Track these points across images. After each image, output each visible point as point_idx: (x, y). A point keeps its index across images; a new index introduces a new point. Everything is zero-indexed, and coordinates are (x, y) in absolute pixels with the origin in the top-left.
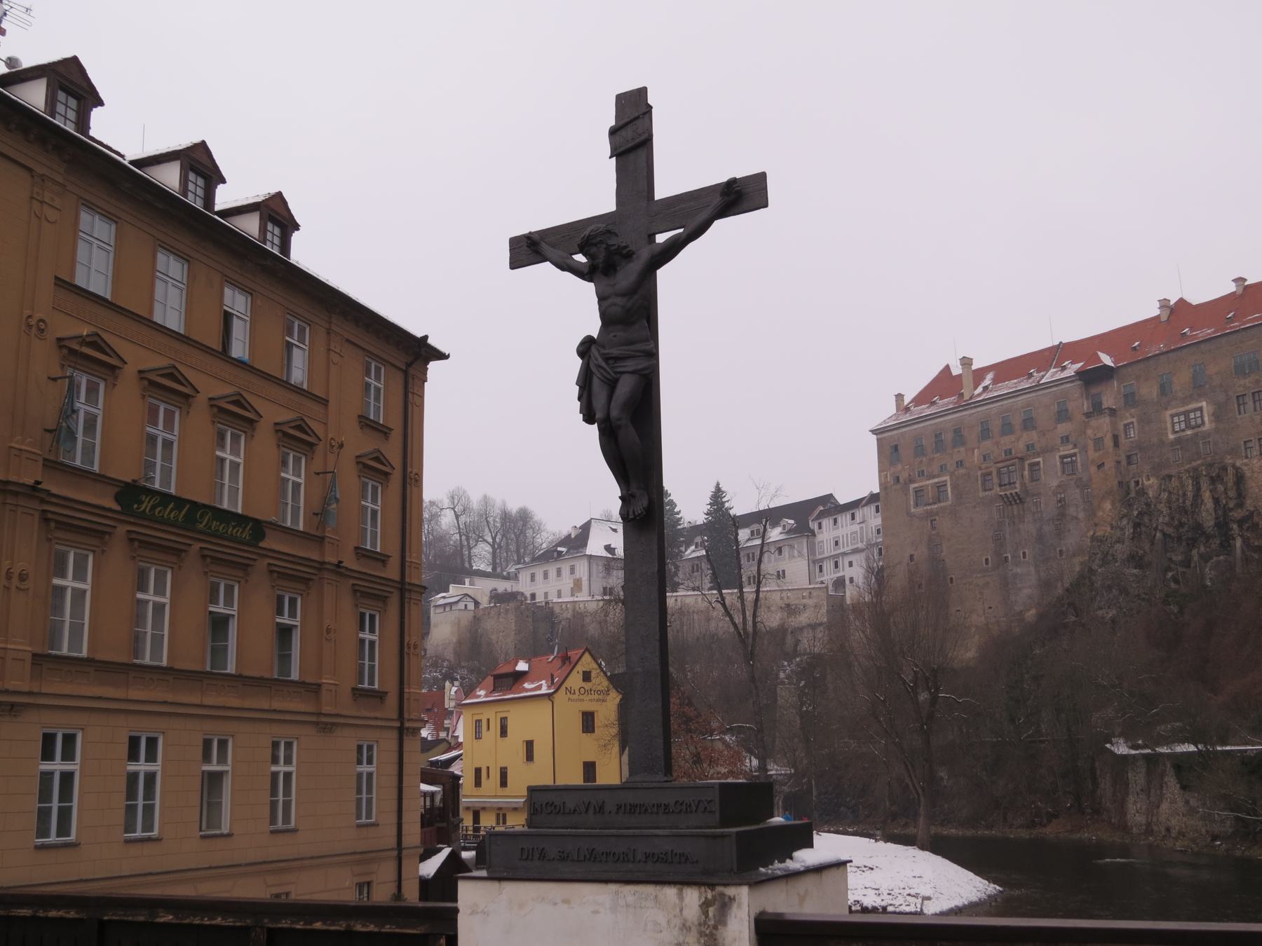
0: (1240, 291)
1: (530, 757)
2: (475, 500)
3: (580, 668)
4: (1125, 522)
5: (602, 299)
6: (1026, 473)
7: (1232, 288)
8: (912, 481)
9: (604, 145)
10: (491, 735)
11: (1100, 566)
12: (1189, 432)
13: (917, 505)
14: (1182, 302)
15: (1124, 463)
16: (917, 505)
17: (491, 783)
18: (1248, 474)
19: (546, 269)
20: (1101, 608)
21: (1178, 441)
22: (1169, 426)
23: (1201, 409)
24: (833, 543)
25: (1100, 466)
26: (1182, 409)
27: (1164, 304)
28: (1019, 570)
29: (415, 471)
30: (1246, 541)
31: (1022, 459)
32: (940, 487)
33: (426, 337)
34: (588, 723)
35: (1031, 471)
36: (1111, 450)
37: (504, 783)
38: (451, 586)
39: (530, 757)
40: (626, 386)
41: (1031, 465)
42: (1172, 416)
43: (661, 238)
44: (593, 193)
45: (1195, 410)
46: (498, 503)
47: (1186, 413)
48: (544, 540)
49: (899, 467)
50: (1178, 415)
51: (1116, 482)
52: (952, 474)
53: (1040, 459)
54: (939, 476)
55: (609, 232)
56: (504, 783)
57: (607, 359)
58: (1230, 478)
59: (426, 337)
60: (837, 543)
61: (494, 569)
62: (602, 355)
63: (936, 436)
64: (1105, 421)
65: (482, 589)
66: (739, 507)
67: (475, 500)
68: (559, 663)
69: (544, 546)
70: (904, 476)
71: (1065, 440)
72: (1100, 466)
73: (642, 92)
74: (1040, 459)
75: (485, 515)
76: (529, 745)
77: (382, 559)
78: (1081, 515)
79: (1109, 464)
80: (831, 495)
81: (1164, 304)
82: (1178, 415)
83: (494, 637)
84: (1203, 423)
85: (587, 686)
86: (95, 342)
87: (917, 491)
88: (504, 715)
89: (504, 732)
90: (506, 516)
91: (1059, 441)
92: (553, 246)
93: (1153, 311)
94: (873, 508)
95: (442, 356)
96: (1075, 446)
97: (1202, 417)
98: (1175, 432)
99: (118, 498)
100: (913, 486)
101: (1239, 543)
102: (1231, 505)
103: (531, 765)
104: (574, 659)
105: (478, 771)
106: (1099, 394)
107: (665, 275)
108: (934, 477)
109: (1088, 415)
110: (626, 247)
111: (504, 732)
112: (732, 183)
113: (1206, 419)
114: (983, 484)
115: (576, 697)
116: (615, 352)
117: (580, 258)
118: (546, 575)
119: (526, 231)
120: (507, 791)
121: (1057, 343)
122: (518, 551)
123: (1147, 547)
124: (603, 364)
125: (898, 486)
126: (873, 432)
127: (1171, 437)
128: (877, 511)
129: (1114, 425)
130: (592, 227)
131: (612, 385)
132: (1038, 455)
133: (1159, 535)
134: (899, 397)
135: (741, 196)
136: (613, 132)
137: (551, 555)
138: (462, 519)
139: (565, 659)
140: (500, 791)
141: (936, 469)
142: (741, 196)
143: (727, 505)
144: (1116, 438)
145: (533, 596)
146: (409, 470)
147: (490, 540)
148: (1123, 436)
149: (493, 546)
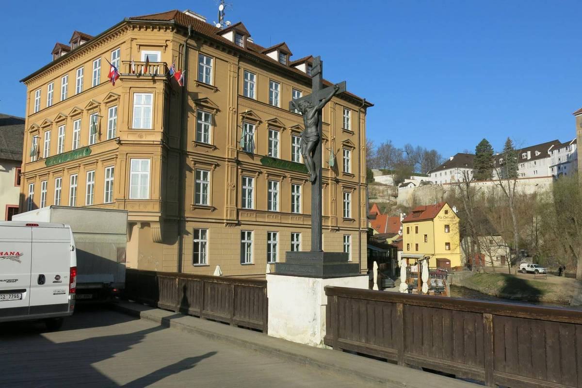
2: (415, 147)
24: (558, 159)
38: (405, 180)
46: (424, 149)
48: (442, 161)
56: (417, 249)
60: (559, 159)
66: (517, 146)
67: (415, 147)
75: (418, 154)
77: (352, 175)
80: (557, 140)
83: (421, 198)
85: (446, 215)
86: (250, 113)
88: (417, 226)
90: (427, 153)
95: (372, 105)
99: (261, 161)
103: (21, 263)
115: (442, 219)
122: (431, 166)
138: (410, 155)
143: (512, 146)
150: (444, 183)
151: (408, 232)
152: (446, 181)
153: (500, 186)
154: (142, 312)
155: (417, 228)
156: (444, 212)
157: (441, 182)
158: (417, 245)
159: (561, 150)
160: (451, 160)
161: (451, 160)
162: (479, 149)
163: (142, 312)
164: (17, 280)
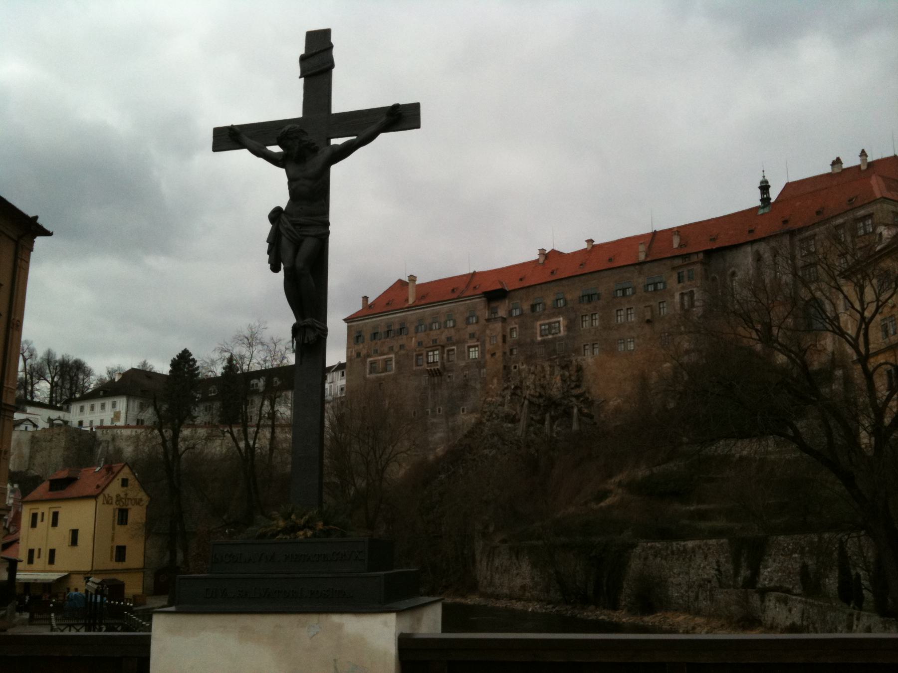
0: (589, 248)
1: (74, 542)
3: (121, 476)
4: (506, 392)
5: (292, 181)
6: (445, 355)
7: (585, 246)
8: (369, 356)
9: (296, 68)
10: (44, 525)
11: (488, 420)
12: (550, 337)
13: (371, 372)
14: (553, 252)
15: (508, 353)
16: (371, 372)
17: (41, 562)
18: (584, 367)
19: (244, 154)
20: (485, 448)
21: (543, 342)
22: (538, 332)
23: (559, 322)
25: (493, 355)
26: (547, 321)
27: (542, 252)
28: (435, 420)
29: (17, 318)
30: (580, 410)
31: (443, 347)
32: (387, 361)
33: (36, 218)
34: (122, 517)
35: (448, 355)
36: (501, 344)
37: (51, 561)
39: (74, 542)
40: (308, 245)
41: (449, 351)
42: (541, 325)
43: (336, 141)
44: (286, 103)
45: (555, 322)
47: (549, 324)
49: (361, 346)
50: (544, 325)
51: (502, 366)
52: (396, 354)
53: (455, 348)
54: (387, 354)
55: (302, 131)
57: (294, 224)
58: (573, 369)
59: (36, 218)
61: (51, 401)
62: (291, 222)
63: (388, 327)
64: (498, 326)
65: (42, 417)
68: (104, 472)
69: (92, 386)
70: (364, 352)
71: (472, 336)
72: (493, 355)
73: (326, 33)
74: (455, 348)
76: (75, 533)
78: (478, 386)
79: (499, 354)
81: (542, 252)
82: (544, 325)
84: (560, 331)
87: (372, 363)
88: (35, 511)
89: (55, 523)
91: (468, 337)
92: (251, 138)
93: (535, 256)
94: (340, 373)
95: (48, 233)
96: (478, 340)
97: (559, 327)
98: (542, 336)
100: (369, 360)
101: (575, 410)
102: (573, 386)
104: (116, 470)
105: (31, 552)
106: (497, 307)
107: (336, 170)
108: (384, 354)
109: (488, 320)
110: (314, 144)
111: (55, 523)
112: (396, 107)
113: (562, 329)
114: (417, 362)
116: (302, 220)
117: (276, 149)
118: (92, 408)
119: (229, 124)
120: (54, 567)
121: (472, 271)
122: (71, 388)
123: (518, 409)
124: (292, 228)
125: (359, 359)
126: (346, 320)
127: (539, 339)
128: (343, 375)
129: (504, 329)
130: (289, 126)
131: (297, 245)
132: (454, 344)
133: (526, 402)
134: (365, 298)
135: (402, 117)
136: (303, 59)
137: (95, 395)
139: (109, 469)
140: (48, 567)
141: (386, 349)
142: (402, 117)
144: (504, 337)
145: (81, 423)
146: (13, 317)
147: (50, 379)
148: (509, 336)
149: (51, 384)
150: (99, 424)
151: (34, 524)
152: (102, 421)
153: (229, 435)
154: (11, 467)
155: (55, 515)
156: (120, 482)
157: (91, 422)
158: (52, 553)
159: (754, 200)
160: (116, 380)
161: (116, 380)
162: (175, 364)
163: (11, 467)
164: (863, 151)
